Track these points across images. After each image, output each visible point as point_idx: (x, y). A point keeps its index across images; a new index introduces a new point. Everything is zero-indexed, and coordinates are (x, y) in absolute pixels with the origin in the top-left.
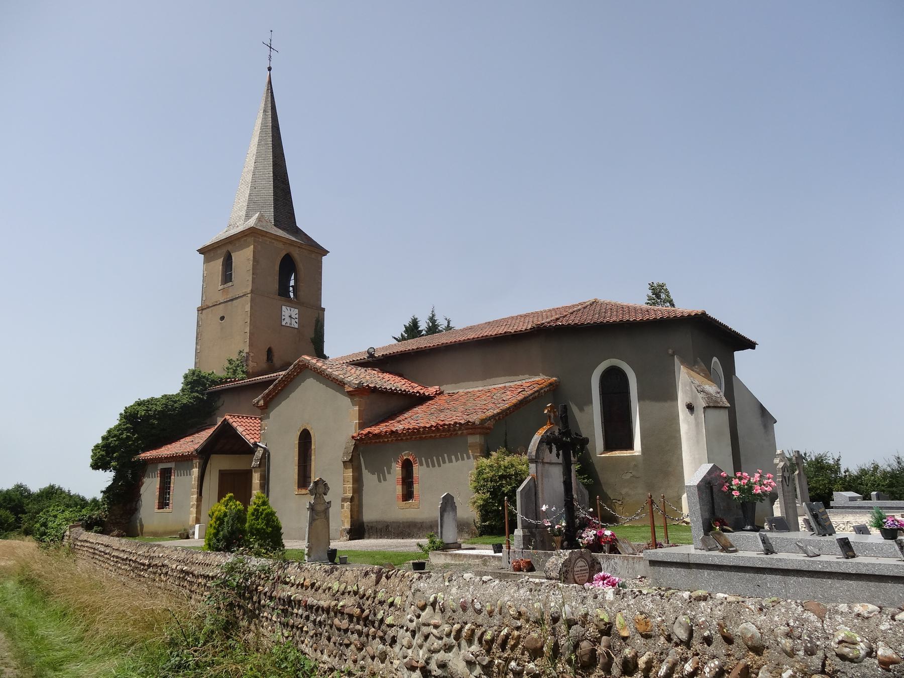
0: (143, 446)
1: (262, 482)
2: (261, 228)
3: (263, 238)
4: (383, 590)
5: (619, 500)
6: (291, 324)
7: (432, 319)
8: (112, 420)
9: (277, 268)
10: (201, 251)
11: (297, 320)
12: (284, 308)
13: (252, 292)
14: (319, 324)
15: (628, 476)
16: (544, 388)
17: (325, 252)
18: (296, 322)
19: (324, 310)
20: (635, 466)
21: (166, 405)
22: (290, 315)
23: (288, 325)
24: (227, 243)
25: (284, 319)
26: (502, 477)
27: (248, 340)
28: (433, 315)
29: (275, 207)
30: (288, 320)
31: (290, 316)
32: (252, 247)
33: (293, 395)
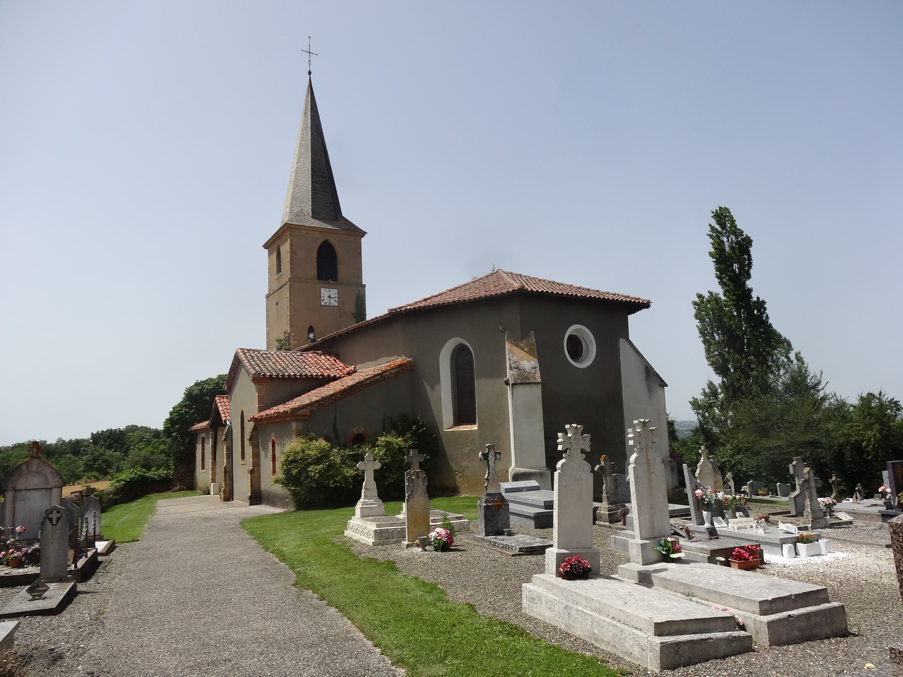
0: (198, 418)
1: (228, 452)
2: (295, 223)
3: (299, 231)
4: (449, 532)
5: (460, 472)
6: (330, 303)
8: (178, 397)
9: (315, 255)
10: (266, 246)
11: (336, 299)
12: (323, 290)
15: (467, 450)
16: (389, 370)
17: (363, 234)
18: (335, 301)
19: (364, 286)
20: (473, 440)
22: (329, 295)
23: (328, 304)
24: (276, 239)
25: (323, 300)
26: (292, 462)
27: (289, 322)
29: (312, 201)
31: (329, 297)
32: (289, 240)
33: (239, 381)
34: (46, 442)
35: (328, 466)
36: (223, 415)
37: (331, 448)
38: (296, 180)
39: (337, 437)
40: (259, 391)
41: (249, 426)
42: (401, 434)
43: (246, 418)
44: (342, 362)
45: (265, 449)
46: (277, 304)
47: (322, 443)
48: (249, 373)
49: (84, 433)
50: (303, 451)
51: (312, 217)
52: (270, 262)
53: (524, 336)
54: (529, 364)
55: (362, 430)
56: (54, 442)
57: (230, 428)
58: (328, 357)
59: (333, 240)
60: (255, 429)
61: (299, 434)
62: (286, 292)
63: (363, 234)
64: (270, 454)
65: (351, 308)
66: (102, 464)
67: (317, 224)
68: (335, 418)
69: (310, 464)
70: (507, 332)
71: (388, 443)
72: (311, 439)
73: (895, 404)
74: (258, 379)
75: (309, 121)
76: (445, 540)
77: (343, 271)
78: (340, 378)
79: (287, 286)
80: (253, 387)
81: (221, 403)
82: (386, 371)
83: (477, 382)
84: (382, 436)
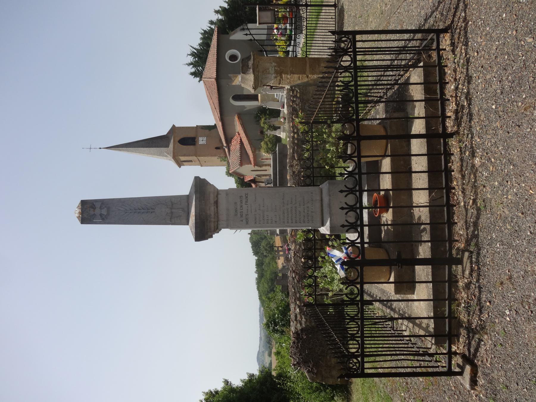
2: (172, 154)
7: (189, 64)
9: (185, 146)
10: (180, 167)
12: (200, 143)
13: (196, 157)
14: (204, 128)
17: (174, 126)
21: (239, 183)
22: (202, 141)
28: (187, 64)
30: (204, 142)
31: (202, 141)
34: (256, 278)
35: (269, 141)
36: (252, 178)
37: (264, 141)
38: (151, 154)
39: (261, 139)
40: (245, 165)
41: (257, 168)
42: (261, 119)
43: (254, 169)
44: (234, 137)
45: (264, 162)
46: (205, 162)
47: (262, 143)
48: (239, 168)
49: (254, 259)
50: (264, 149)
51: (168, 147)
52: (187, 165)
53: (230, 78)
54: (239, 78)
55: (259, 131)
56: (257, 275)
57: (256, 175)
58: (232, 142)
59: (178, 139)
60: (257, 166)
61: (260, 151)
62: (201, 158)
63: (174, 126)
64: (265, 160)
65: (207, 131)
66: (268, 247)
67: (171, 145)
68: (255, 140)
69: (268, 147)
70: (229, 84)
71: (263, 123)
72: (261, 147)
74: (241, 164)
75: (123, 148)
77: (191, 135)
78: (241, 138)
79: (198, 157)
80: (243, 167)
81: (247, 179)
82: (240, 123)
83: (245, 94)
84: (261, 125)
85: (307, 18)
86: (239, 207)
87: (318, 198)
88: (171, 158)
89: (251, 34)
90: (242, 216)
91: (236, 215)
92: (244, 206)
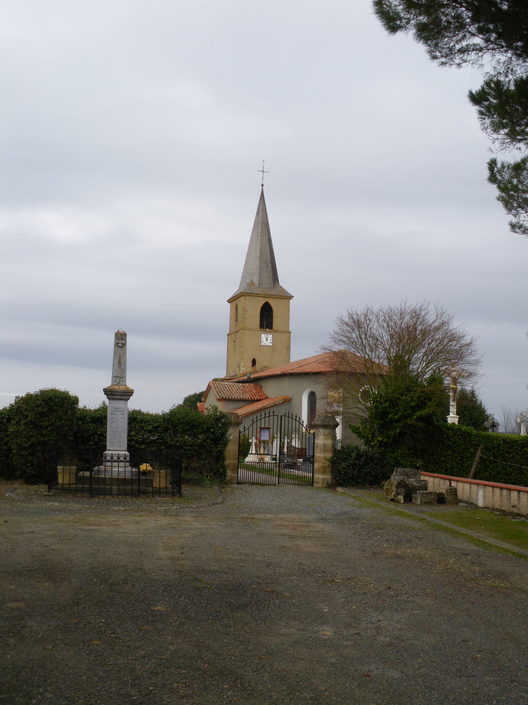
10: (230, 301)
12: (263, 335)
54: (82, 472)
73: (374, 2)
76: (394, 420)
85: (263, 463)
86: (119, 410)
87: (121, 449)
88: (242, 290)
89: (257, 421)
90: (114, 411)
91: (115, 409)
92: (119, 413)
